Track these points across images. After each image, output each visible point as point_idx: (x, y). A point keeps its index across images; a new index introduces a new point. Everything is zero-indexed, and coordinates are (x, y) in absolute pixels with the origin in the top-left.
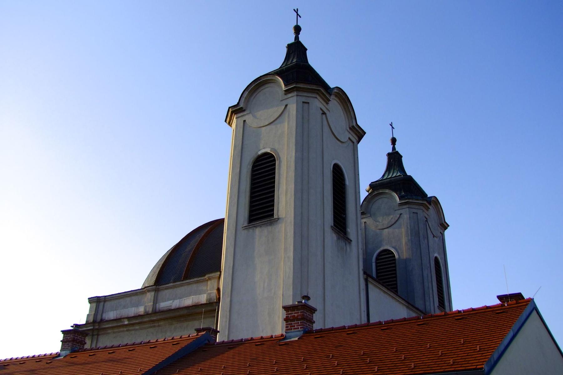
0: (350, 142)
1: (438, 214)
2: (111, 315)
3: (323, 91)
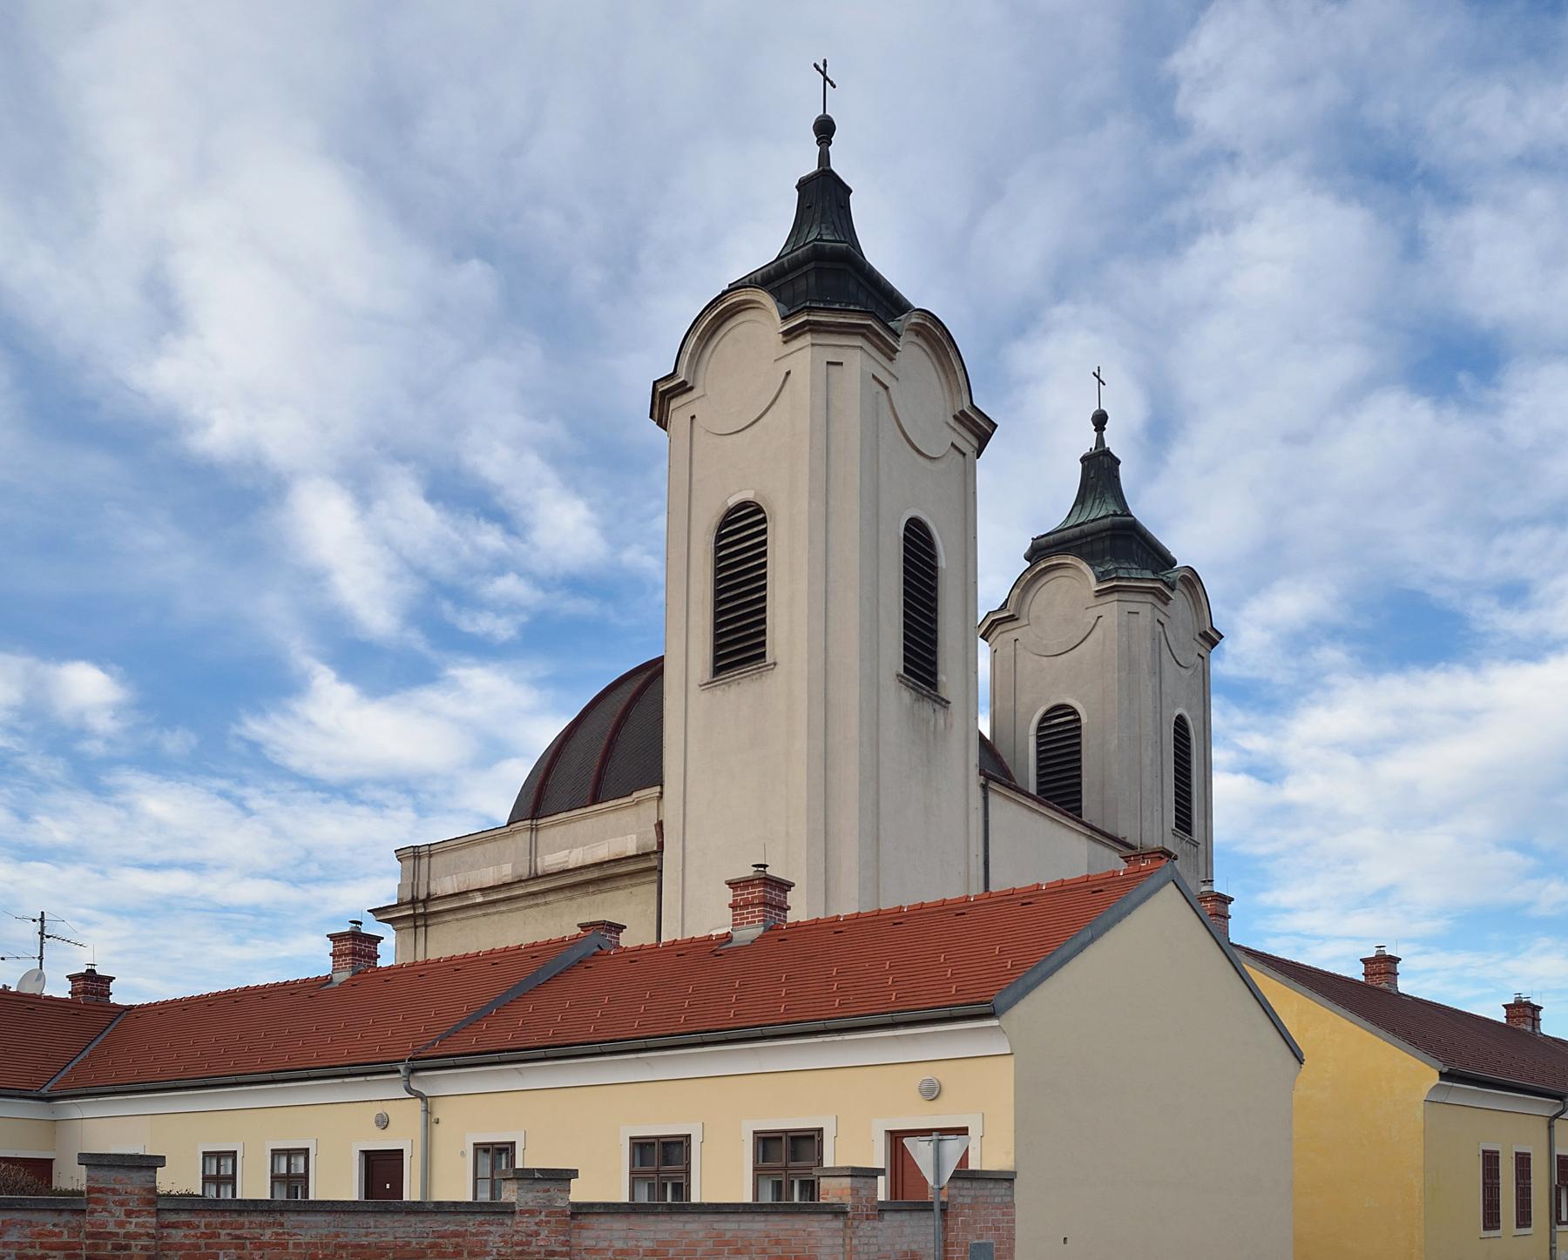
0: (956, 453)
1: (1196, 610)
2: (445, 885)
3: (876, 327)
